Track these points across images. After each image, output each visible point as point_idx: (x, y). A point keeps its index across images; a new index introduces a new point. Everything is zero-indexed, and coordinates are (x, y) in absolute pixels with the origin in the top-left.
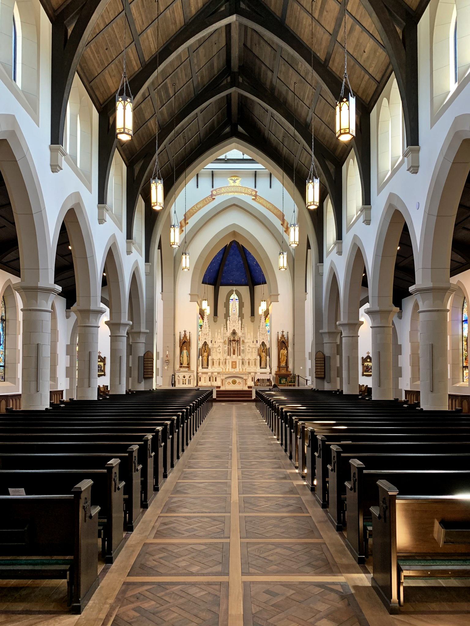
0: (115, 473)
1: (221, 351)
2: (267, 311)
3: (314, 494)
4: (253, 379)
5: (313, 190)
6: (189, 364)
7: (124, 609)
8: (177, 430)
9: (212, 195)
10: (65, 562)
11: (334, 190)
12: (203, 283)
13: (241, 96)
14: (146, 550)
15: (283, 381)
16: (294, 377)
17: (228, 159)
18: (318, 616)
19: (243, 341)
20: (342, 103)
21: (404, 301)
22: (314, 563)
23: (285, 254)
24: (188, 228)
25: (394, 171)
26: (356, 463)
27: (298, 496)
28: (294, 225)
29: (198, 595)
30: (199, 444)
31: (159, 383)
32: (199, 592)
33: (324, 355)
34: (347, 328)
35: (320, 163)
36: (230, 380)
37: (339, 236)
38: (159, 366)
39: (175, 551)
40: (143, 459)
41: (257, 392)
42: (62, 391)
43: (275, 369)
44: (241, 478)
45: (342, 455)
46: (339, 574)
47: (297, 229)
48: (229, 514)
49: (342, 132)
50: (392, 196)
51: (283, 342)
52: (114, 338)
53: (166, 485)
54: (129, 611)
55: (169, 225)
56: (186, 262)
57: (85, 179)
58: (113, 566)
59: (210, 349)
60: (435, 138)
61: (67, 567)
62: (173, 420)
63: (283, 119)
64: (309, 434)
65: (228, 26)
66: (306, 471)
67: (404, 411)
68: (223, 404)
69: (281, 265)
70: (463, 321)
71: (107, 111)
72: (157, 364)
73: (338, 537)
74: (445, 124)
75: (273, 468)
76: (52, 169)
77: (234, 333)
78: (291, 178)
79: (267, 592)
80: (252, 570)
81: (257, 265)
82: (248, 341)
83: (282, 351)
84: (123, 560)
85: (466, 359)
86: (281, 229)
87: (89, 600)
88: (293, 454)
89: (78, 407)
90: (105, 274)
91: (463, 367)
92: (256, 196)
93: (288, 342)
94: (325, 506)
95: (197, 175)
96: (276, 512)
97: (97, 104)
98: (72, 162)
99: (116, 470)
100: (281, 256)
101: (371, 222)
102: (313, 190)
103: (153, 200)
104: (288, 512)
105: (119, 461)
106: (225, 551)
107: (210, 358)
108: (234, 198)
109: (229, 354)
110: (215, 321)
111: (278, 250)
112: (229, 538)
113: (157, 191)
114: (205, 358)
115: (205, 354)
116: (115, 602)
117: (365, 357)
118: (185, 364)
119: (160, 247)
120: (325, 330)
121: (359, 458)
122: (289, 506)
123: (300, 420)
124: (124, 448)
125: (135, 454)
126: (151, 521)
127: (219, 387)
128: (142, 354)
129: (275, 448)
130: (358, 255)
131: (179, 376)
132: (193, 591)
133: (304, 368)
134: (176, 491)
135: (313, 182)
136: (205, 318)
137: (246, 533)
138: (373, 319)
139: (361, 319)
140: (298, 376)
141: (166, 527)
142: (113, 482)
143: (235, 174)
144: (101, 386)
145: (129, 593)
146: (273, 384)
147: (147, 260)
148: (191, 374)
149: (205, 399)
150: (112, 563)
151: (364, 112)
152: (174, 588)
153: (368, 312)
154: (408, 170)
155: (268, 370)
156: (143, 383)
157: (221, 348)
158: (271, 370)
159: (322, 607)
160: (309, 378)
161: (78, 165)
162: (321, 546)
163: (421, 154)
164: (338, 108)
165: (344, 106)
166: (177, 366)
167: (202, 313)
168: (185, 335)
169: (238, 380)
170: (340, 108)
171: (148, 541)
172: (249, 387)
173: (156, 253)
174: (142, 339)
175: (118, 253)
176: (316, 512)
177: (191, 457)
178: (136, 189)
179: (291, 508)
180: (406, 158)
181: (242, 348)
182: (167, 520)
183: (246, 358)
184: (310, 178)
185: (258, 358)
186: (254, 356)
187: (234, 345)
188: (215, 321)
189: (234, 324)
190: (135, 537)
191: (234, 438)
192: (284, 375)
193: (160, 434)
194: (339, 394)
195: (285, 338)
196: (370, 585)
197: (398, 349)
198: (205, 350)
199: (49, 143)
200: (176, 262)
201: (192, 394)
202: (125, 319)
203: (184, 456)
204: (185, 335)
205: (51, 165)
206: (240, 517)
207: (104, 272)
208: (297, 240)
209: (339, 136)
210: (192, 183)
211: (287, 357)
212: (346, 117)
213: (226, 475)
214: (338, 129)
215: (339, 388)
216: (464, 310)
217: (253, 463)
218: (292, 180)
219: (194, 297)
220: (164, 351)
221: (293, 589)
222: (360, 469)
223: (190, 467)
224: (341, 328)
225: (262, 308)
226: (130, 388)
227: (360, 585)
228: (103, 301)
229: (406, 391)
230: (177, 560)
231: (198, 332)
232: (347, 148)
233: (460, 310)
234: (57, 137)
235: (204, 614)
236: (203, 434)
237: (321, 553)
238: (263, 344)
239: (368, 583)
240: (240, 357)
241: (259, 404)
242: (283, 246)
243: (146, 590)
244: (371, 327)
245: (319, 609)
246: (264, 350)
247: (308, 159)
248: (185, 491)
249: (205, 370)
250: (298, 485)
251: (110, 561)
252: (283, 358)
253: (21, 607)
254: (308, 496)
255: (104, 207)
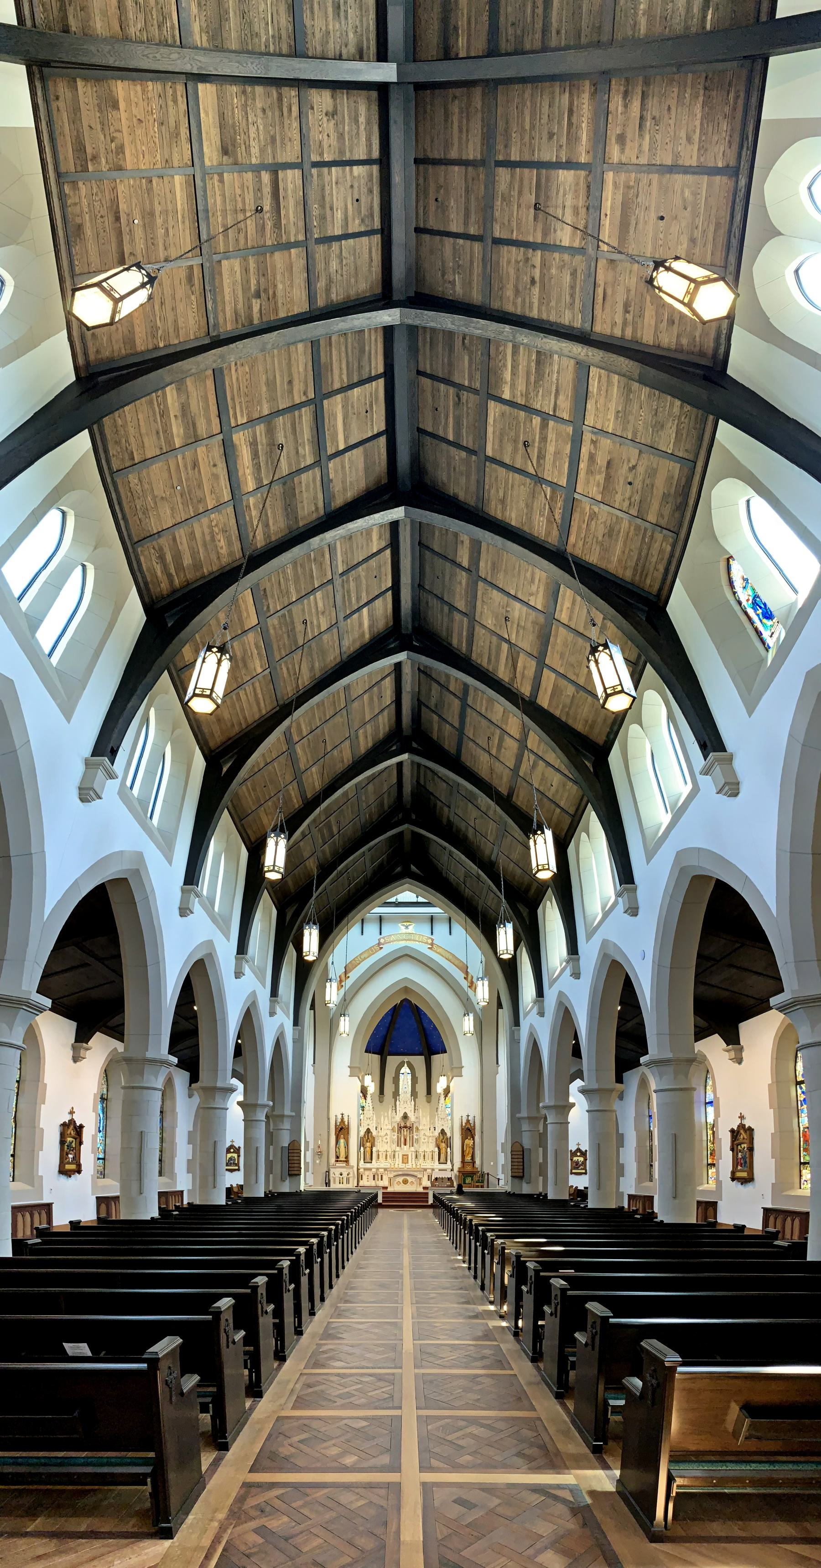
0: (227, 1320)
1: (388, 1140)
2: (448, 1087)
3: (518, 1341)
4: (429, 1177)
5: (505, 937)
6: (347, 1157)
7: (239, 1529)
8: (328, 1251)
9: (379, 944)
10: (145, 1462)
11: (530, 936)
12: (366, 1051)
13: (413, 833)
14: (280, 1429)
15: (468, 1180)
16: (483, 1175)
17: (400, 903)
18: (538, 1546)
19: (417, 1129)
20: (597, 654)
21: (626, 1075)
22: (527, 1452)
24: (348, 983)
25: (606, 915)
26: (558, 1283)
27: (495, 1343)
28: (482, 979)
29: (353, 1506)
30: (359, 1267)
31: (308, 1182)
32: (357, 1500)
33: (523, 1148)
34: (553, 1111)
35: (510, 907)
36: (401, 1179)
37: (540, 992)
38: (309, 1159)
39: (323, 1429)
40: (295, 1277)
41: (434, 1196)
42: (182, 1192)
43: (458, 1164)
44: (415, 1315)
45: (542, 1274)
46: (567, 1471)
47: (486, 983)
48: (400, 1371)
49: (540, 868)
50: (605, 943)
51: (468, 1129)
52: (249, 1122)
53: (313, 1327)
54: (248, 1535)
55: (326, 979)
56: (345, 1025)
57: (221, 922)
58: (230, 1455)
59: (374, 1138)
60: (655, 876)
61: (148, 1470)
62: (330, 1231)
63: (463, 857)
64: (514, 1259)
65: (400, 765)
66: (505, 1308)
67: (632, 1223)
68: (392, 1210)
69: (466, 1029)
70: (706, 1103)
71: (256, 851)
72: (306, 1157)
73: (559, 1408)
74: (665, 860)
75: (459, 1303)
76: (80, 794)
77: (405, 1117)
78: (476, 923)
79: (460, 1502)
80: (435, 1463)
81: (435, 1028)
83: (467, 1141)
84: (245, 1445)
85: (711, 1154)
86: (465, 984)
87: (187, 1514)
88: (487, 1282)
89: (201, 1213)
90: (240, 1041)
91: (708, 1165)
92: (432, 944)
93: (474, 1129)
94: (536, 1357)
95: (363, 920)
96: (466, 1368)
97: (247, 843)
98: (209, 904)
99: (262, 1291)
100: (466, 1018)
101: (582, 976)
102: (505, 937)
103: (305, 948)
104: (484, 1367)
105: (265, 1279)
106: (394, 1427)
107: (374, 1149)
108: (406, 947)
109: (399, 1145)
110: (381, 1101)
111: (462, 1011)
112: (400, 1408)
113: (311, 938)
114: (368, 1149)
115: (368, 1144)
116: (227, 1519)
117: (573, 1150)
118: (342, 1158)
119: (313, 1007)
120: (524, 1113)
121: (563, 1278)
122: (483, 1358)
123: (498, 1237)
124: (272, 1264)
125: (286, 1271)
126: (288, 1381)
127: (386, 1188)
128: (286, 1144)
129: (460, 1273)
130: (566, 1016)
131: (335, 1173)
132: (346, 1498)
133: (496, 1164)
134: (328, 1334)
135: (505, 926)
136: (369, 1097)
137: (425, 1401)
138: (590, 1100)
139: (571, 1100)
140: (488, 1174)
141: (310, 1390)
142: (260, 1306)
143: (407, 919)
144: (235, 1185)
145: (251, 1502)
146: (455, 1184)
147: (296, 1022)
148: (350, 1171)
149: (368, 1204)
150: (228, 1450)
151: (561, 846)
152: (318, 1495)
153: (583, 1091)
154: (625, 912)
155: (448, 1166)
156: (287, 1182)
157: (388, 1137)
158: (453, 1166)
159: (545, 1529)
160: (501, 1176)
161: (216, 909)
162: (533, 1424)
163: (639, 892)
164: (592, 665)
165: (540, 839)
166: (333, 1160)
167: (364, 1091)
168: (342, 1119)
169: (410, 1179)
170: (535, 841)
171: (284, 1413)
172: (424, 1188)
173: (307, 1015)
174: (287, 1125)
175: (258, 1014)
176: (523, 1369)
177: (349, 1286)
178: (286, 936)
179: (486, 1362)
180: (620, 899)
181: (415, 1137)
182: (312, 1380)
183: (421, 1150)
184: (501, 922)
185: (436, 1150)
186: (432, 1147)
188: (381, 1101)
189: (405, 1104)
190: (264, 1409)
191: (406, 1259)
192: (470, 1173)
193: (315, 1247)
194: (540, 1199)
196: (614, 1490)
197: (621, 1140)
198: (368, 1138)
199: (182, 884)
200: (333, 1026)
201: (352, 1197)
202: (264, 1098)
203: (339, 1284)
204: (342, 1119)
205: (180, 908)
206: (416, 1375)
207: (239, 1037)
208: (487, 997)
209: (537, 872)
210: (355, 930)
211: (473, 1149)
212: (542, 852)
213: (396, 1312)
214: (534, 865)
215: (541, 1190)
216: (708, 1087)
217: (432, 1295)
218: (479, 927)
219: (355, 1070)
220: (315, 1141)
221: (498, 1497)
222: (563, 1291)
223: (346, 1302)
224: (544, 1112)
225: (440, 1085)
226: (271, 1188)
227: (599, 1489)
228: (235, 1074)
229: (629, 1196)
230: (325, 1444)
231: (359, 1115)
232: (543, 887)
233: (702, 1088)
234: (192, 876)
235: (363, 1540)
236: (365, 1253)
237: (535, 1434)
238: (443, 1132)
239: (611, 1487)
240: (412, 1149)
241: (439, 1211)
242: (468, 1006)
243: (277, 1497)
244: (588, 1111)
245: (540, 1532)
246: (444, 1140)
247: (496, 901)
248: (340, 1336)
249: (368, 1166)
250: (494, 1327)
251: (224, 1447)
252: (468, 1151)
253: (83, 1525)
254: (509, 1345)
255: (192, 890)
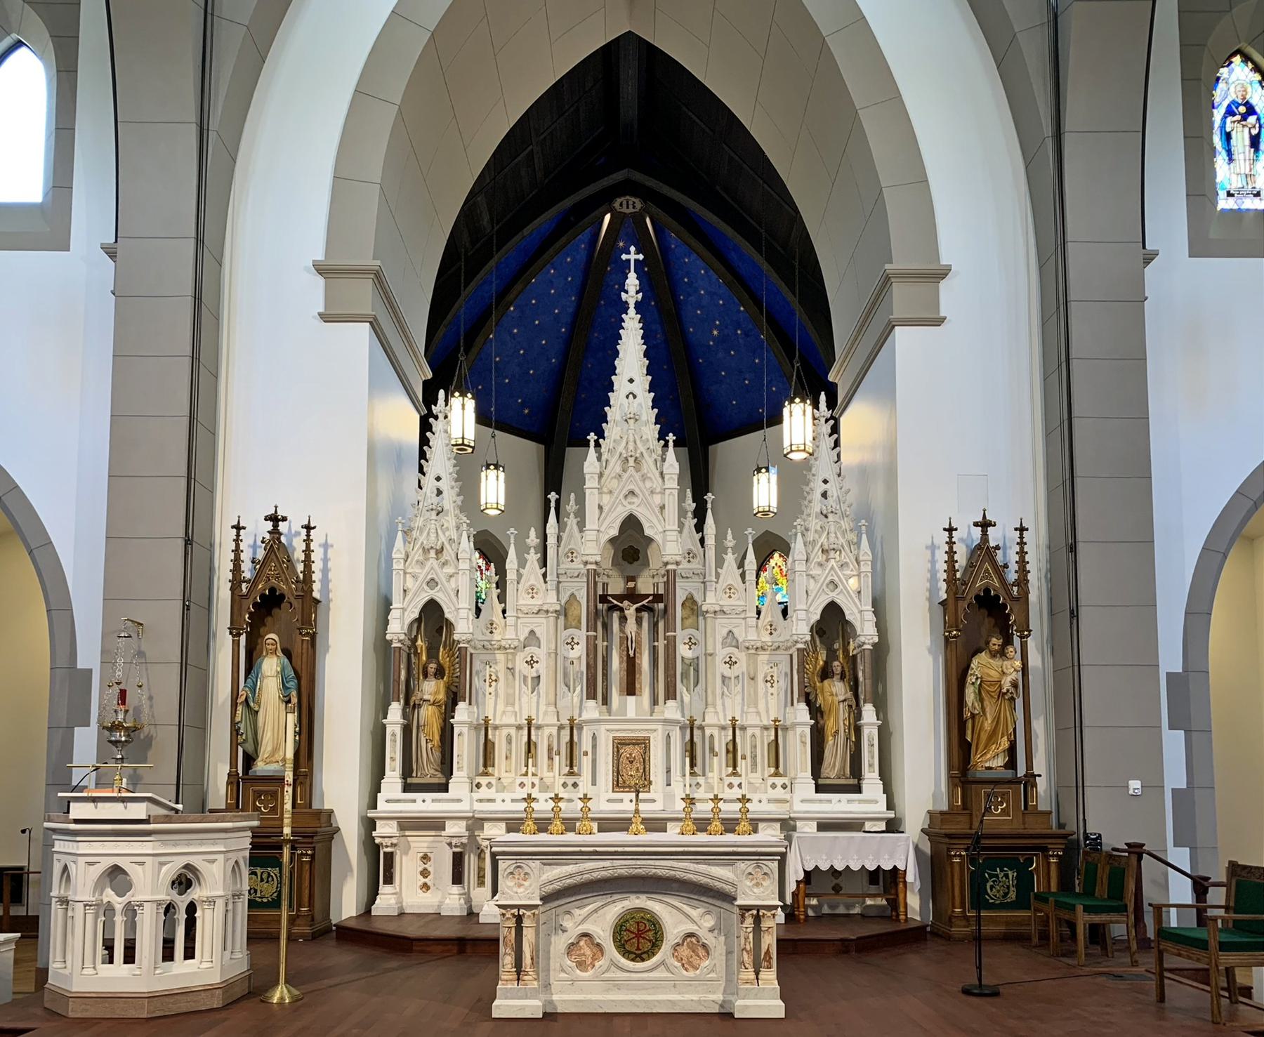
19: (692, 605)
23: (773, 470)
36: (600, 919)
77: (631, 545)
82: (726, 602)
93: (1024, 598)
114: (428, 715)
115: (431, 689)
157: (540, 653)
169: (676, 918)
181: (683, 651)
183: (714, 719)
185: (802, 713)
187: (631, 626)
195: (1000, 570)
198: (425, 660)
240: (671, 710)
246: (837, 658)
249: (425, 804)
